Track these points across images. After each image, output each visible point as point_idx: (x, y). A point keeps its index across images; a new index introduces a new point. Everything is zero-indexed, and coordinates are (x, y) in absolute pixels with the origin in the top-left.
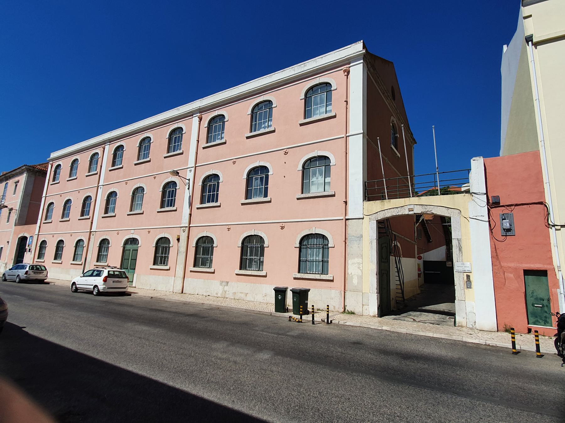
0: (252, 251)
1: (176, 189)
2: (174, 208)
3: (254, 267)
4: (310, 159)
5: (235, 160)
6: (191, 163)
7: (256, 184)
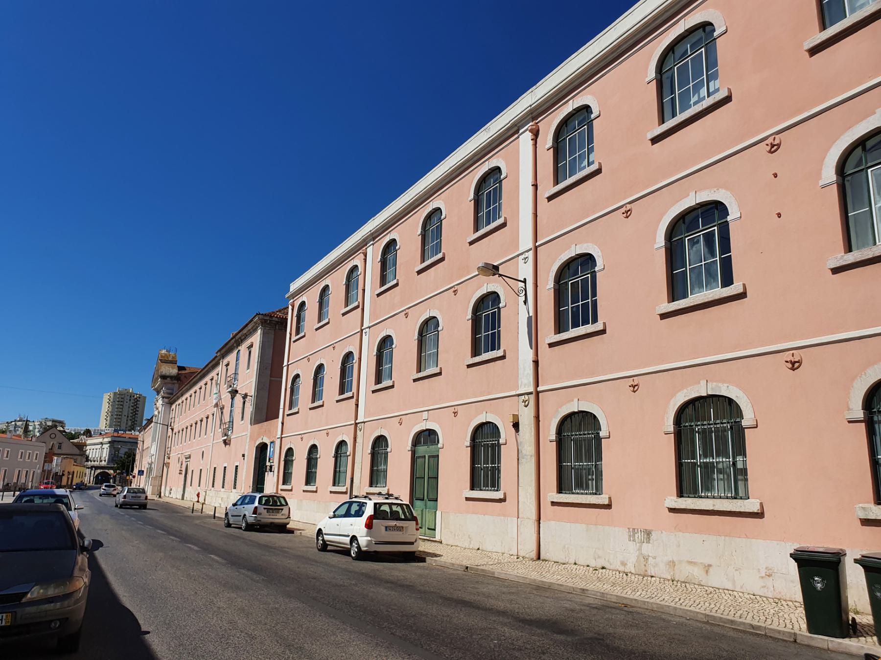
0: (708, 442)
1: (499, 309)
2: (500, 353)
3: (719, 485)
4: (682, 218)
5: (629, 207)
6: (526, 242)
7: (695, 255)
